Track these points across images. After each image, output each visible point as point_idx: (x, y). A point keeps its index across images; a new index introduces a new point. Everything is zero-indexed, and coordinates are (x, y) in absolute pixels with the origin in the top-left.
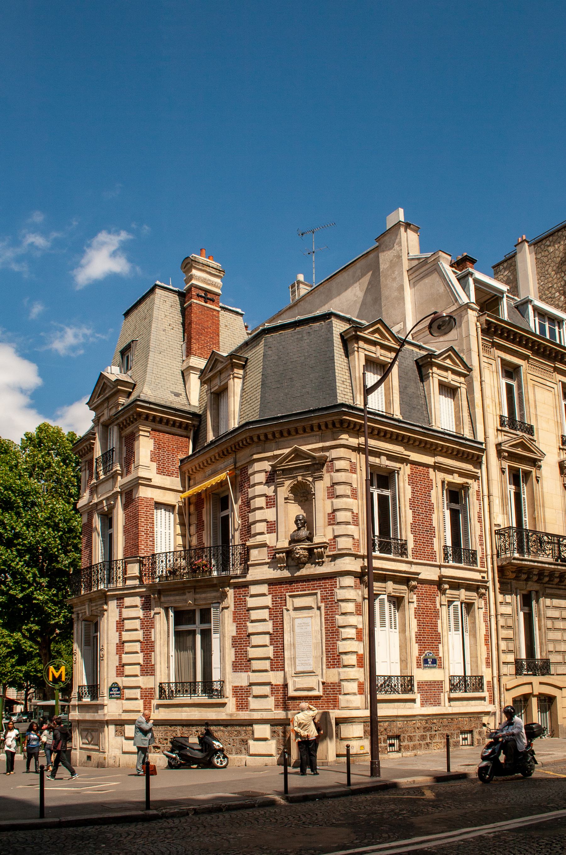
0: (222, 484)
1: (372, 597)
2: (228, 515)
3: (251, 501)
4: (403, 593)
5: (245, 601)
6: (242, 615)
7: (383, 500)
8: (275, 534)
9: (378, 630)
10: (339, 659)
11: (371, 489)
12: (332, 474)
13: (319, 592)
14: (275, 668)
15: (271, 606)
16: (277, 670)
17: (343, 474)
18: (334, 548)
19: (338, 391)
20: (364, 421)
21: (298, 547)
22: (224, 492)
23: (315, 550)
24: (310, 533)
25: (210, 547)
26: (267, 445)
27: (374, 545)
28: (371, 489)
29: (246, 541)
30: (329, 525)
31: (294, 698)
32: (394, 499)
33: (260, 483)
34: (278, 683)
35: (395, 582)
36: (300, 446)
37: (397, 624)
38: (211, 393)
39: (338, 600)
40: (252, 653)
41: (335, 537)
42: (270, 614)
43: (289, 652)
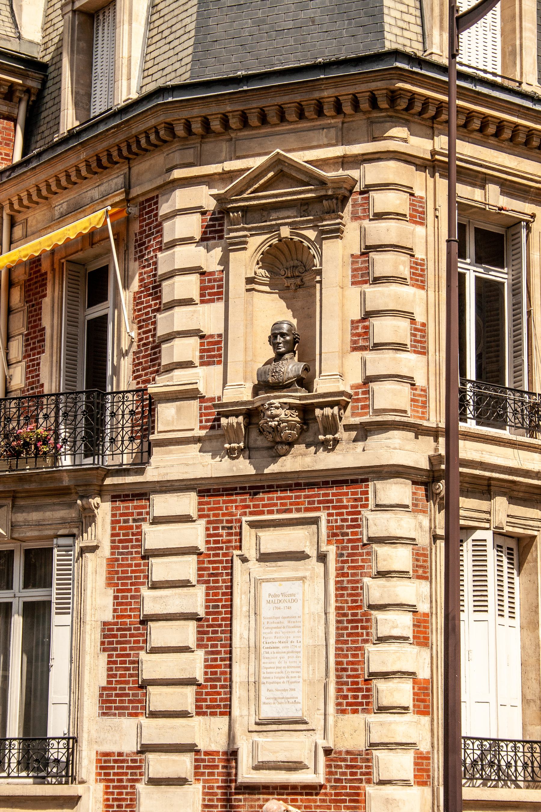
0: (93, 238)
1: (454, 536)
2: (106, 315)
3: (164, 346)
4: (531, 528)
5: (140, 533)
6: (130, 569)
7: (489, 293)
8: (220, 367)
9: (467, 618)
10: (368, 690)
11: (461, 265)
12: (366, 223)
13: (323, 515)
14: (208, 707)
15: (202, 547)
16: (213, 714)
17: (392, 224)
18: (363, 407)
19: (387, 19)
20: (449, 95)
21: (276, 402)
22: (97, 257)
23: (318, 412)
24: (306, 369)
25: (58, 395)
26: (209, 147)
27: (463, 403)
28: (461, 265)
29: (147, 381)
30: (354, 349)
31: (252, 789)
32: (516, 291)
33: (186, 241)
34: (213, 748)
35: (513, 500)
36: (289, 151)
37: (517, 606)
38: (74, 11)
39: (370, 539)
40: (152, 666)
41: (368, 380)
42: (199, 569)
43: (244, 666)
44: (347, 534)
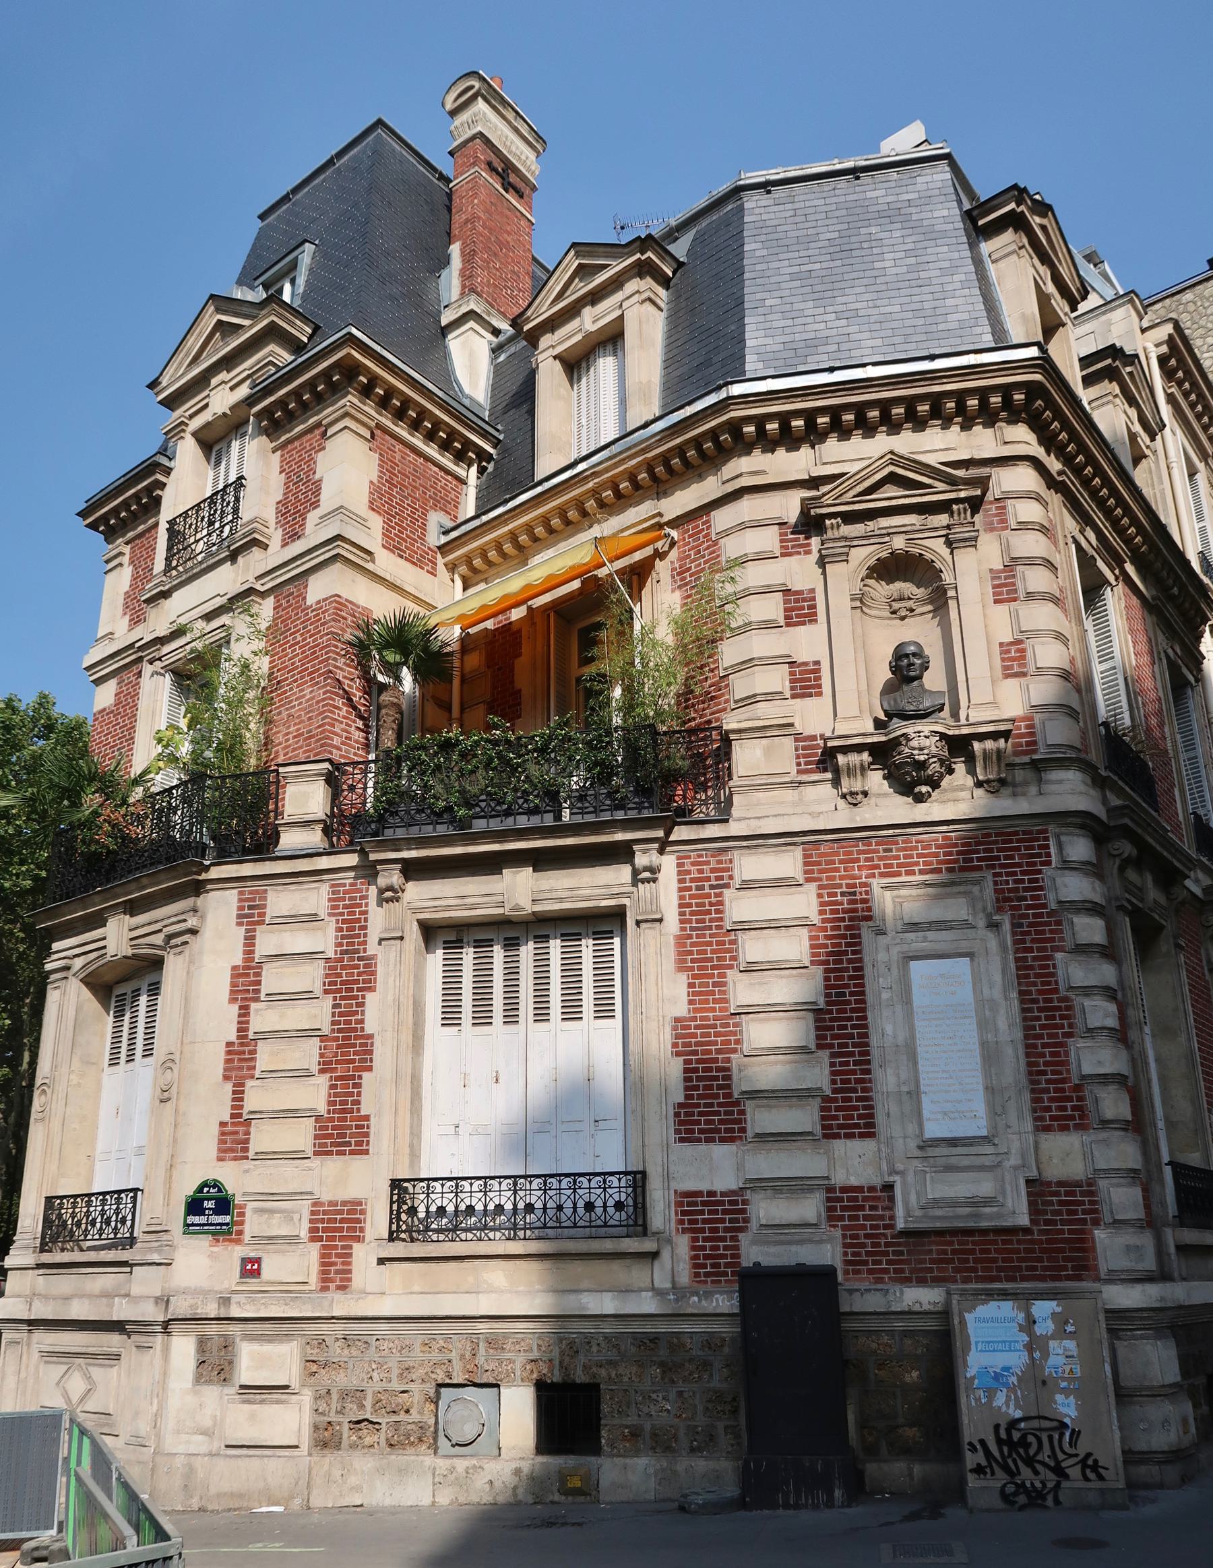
14: (840, 1127)
44: (1025, 899)
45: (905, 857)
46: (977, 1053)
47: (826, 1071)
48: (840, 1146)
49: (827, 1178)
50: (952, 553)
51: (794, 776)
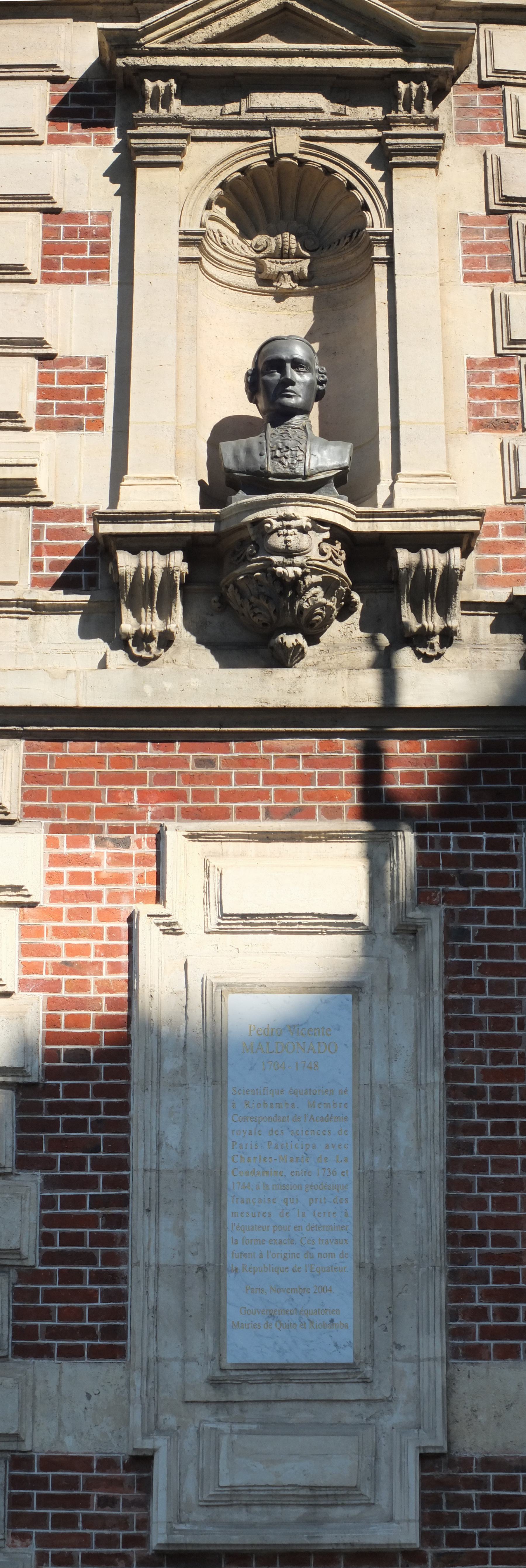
14: (52, 1333)
16: (71, 1353)
23: (404, 557)
44: (478, 880)
45: (241, 779)
46: (349, 1194)
47: (33, 1215)
48: (48, 1372)
49: (17, 1437)
50: (388, 179)
51: (24, 590)
